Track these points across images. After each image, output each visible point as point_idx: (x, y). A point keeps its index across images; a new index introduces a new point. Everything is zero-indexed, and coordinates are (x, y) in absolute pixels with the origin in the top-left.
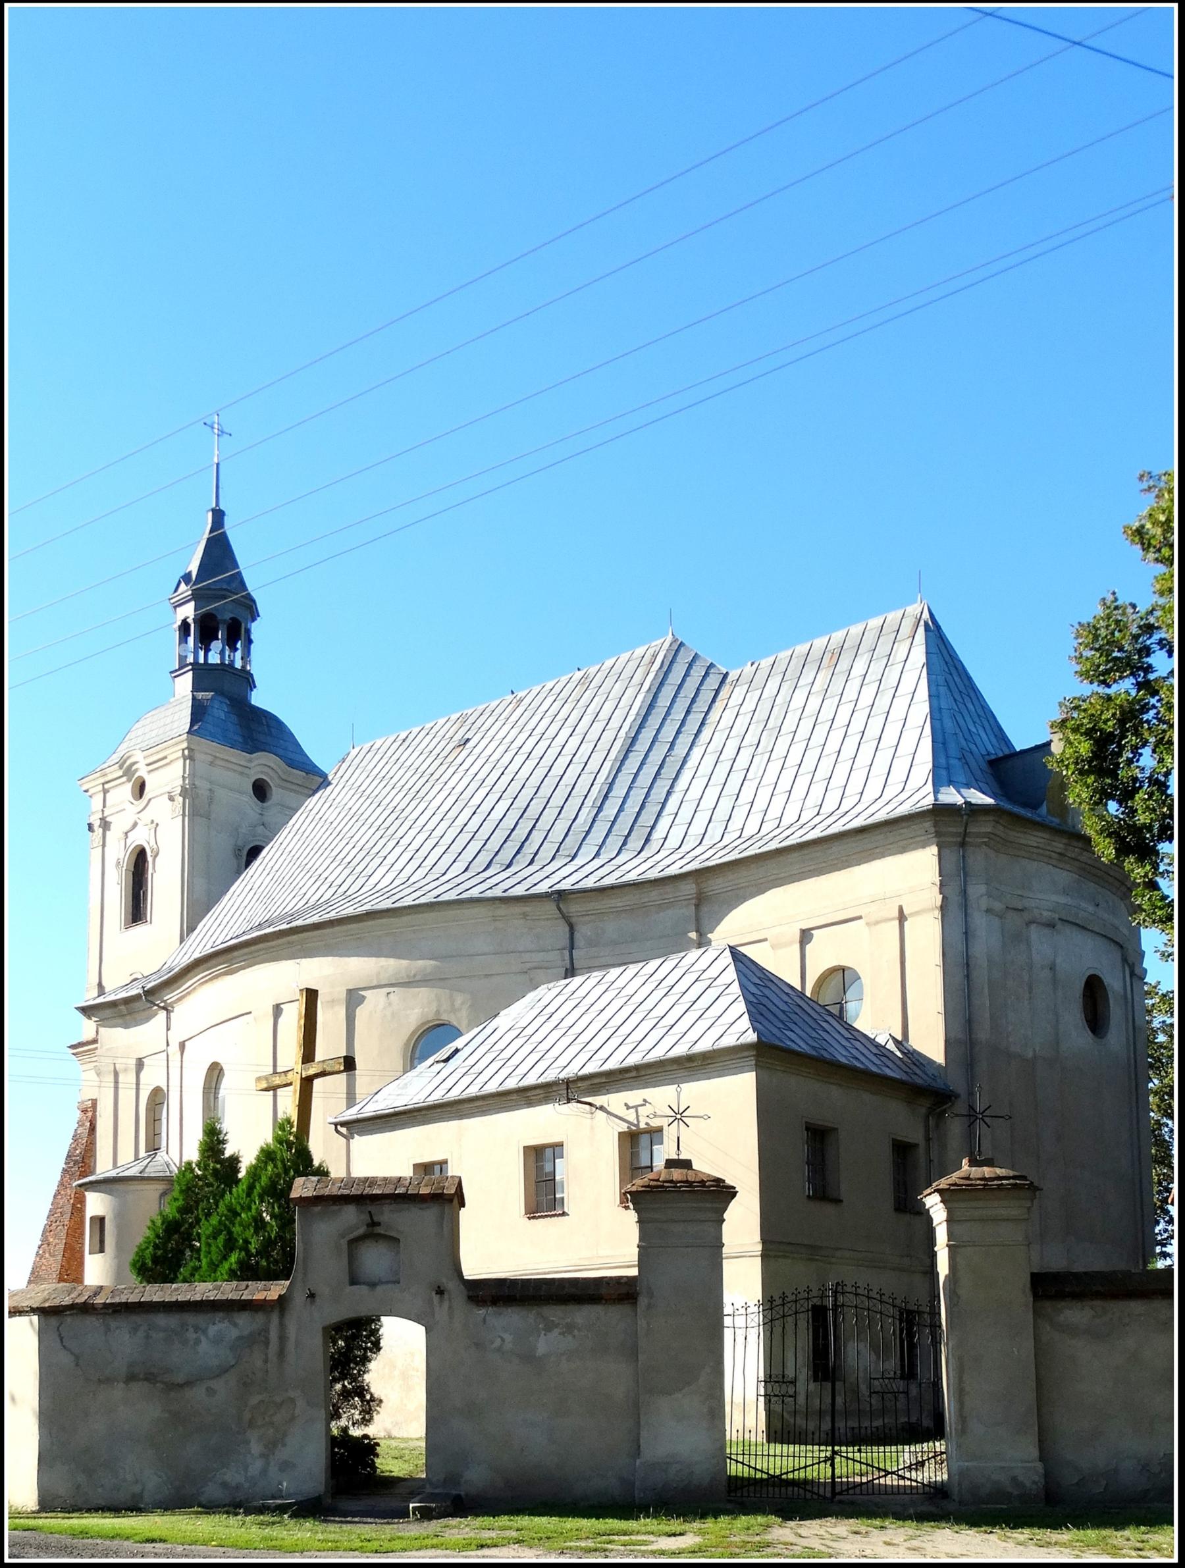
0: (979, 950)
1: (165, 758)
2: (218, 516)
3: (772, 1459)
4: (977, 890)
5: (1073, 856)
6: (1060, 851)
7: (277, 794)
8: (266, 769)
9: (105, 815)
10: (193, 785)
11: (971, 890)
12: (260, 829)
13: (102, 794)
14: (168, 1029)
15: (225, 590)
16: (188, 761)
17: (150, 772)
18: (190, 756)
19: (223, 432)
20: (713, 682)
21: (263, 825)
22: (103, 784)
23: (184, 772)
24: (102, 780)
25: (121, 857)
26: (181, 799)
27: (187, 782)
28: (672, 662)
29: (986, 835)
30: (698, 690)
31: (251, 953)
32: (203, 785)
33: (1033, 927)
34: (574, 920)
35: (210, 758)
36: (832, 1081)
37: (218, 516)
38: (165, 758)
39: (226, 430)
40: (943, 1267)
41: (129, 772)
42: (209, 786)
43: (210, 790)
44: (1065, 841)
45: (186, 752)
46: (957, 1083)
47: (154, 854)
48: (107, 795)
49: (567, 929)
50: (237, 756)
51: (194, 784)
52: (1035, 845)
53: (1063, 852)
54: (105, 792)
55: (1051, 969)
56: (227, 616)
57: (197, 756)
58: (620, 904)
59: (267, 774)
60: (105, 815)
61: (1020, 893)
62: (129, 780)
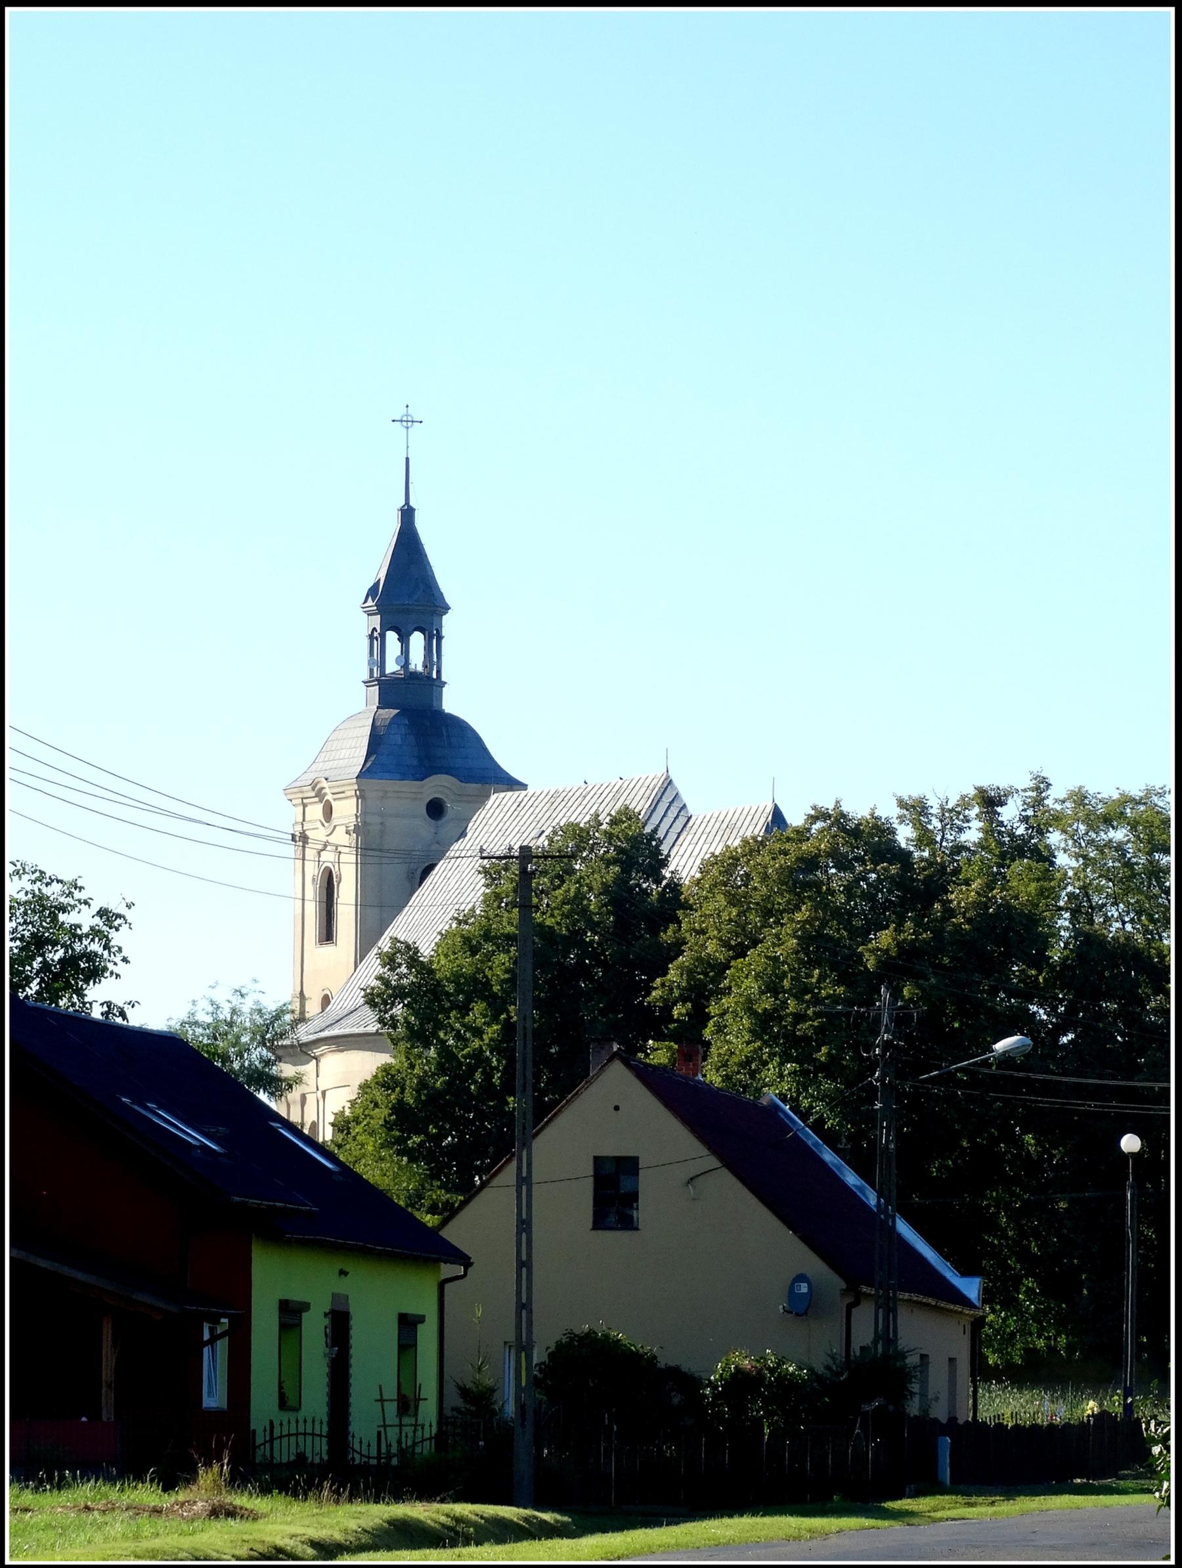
1: (343, 792)
2: (407, 514)
3: (301, 1438)
7: (452, 808)
8: (441, 789)
9: (305, 828)
10: (365, 823)
12: (435, 847)
13: (301, 808)
14: (317, 1076)
16: (360, 801)
17: (335, 800)
18: (361, 796)
20: (682, 820)
21: (437, 843)
22: (302, 799)
23: (357, 812)
24: (300, 795)
25: (316, 874)
26: (355, 835)
27: (359, 820)
28: (659, 801)
30: (668, 832)
31: (585, 797)
32: (374, 820)
37: (407, 514)
38: (343, 792)
39: (409, 430)
40: (904, 1228)
41: (320, 795)
42: (379, 820)
43: (382, 823)
45: (358, 792)
47: (338, 880)
48: (306, 809)
50: (409, 786)
51: (365, 822)
54: (305, 805)
59: (441, 793)
60: (305, 828)
62: (321, 801)
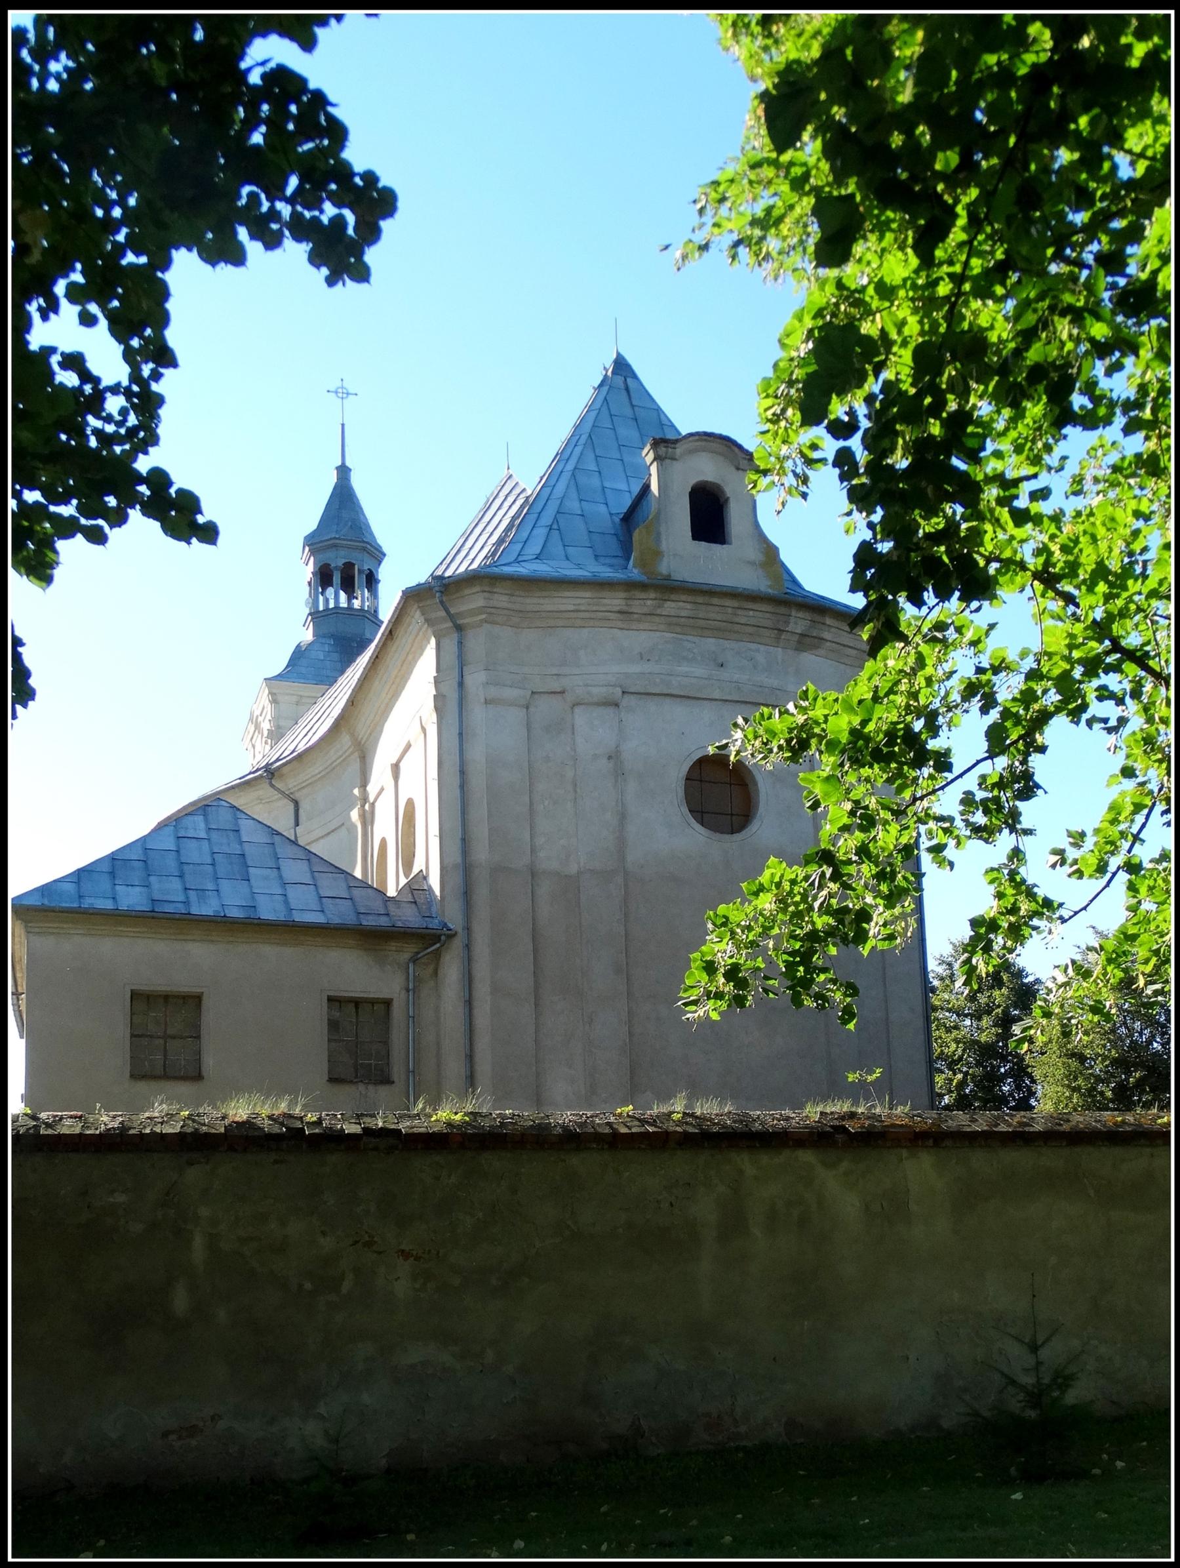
0: (477, 753)
2: (343, 471)
4: (475, 679)
5: (645, 610)
6: (617, 609)
11: (469, 680)
15: (335, 538)
19: (348, 394)
29: (481, 610)
33: (577, 710)
34: (297, 796)
35: (294, 699)
36: (189, 937)
37: (343, 471)
44: (622, 595)
46: (454, 918)
49: (291, 806)
52: (571, 608)
53: (625, 608)
55: (610, 758)
56: (340, 563)
57: (280, 698)
58: (317, 771)
61: (555, 671)
